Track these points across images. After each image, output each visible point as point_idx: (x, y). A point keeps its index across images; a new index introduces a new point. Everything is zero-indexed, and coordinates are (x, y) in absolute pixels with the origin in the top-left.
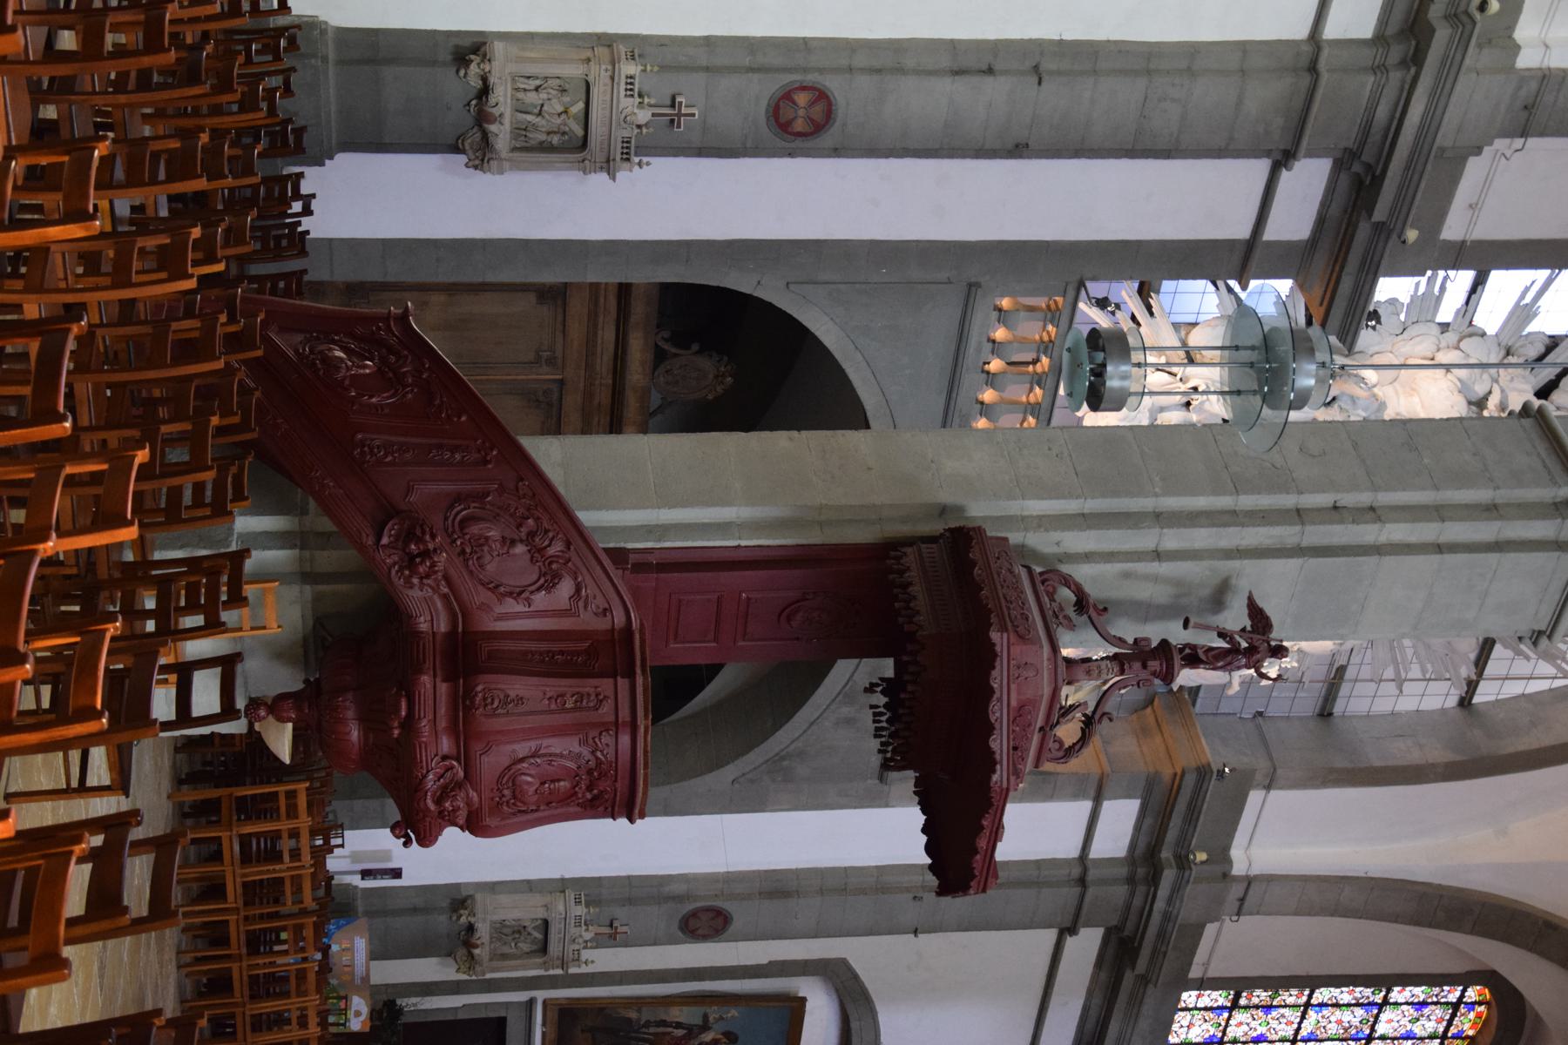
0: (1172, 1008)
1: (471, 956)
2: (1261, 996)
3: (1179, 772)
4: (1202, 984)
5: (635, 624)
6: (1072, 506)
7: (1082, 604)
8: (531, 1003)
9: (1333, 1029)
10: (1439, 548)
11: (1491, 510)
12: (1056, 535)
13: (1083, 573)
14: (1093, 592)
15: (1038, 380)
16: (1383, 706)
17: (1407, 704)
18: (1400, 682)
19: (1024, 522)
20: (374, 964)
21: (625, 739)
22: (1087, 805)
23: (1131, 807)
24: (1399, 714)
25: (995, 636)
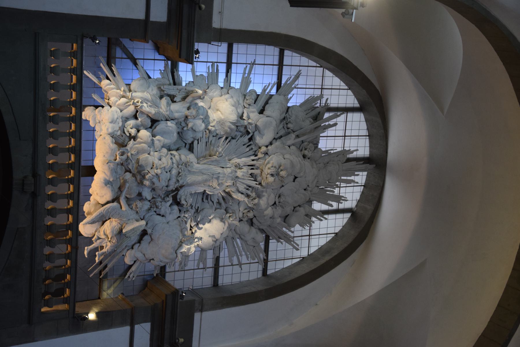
3: (164, 298)
16: (236, 279)
17: (245, 278)
22: (128, 328)
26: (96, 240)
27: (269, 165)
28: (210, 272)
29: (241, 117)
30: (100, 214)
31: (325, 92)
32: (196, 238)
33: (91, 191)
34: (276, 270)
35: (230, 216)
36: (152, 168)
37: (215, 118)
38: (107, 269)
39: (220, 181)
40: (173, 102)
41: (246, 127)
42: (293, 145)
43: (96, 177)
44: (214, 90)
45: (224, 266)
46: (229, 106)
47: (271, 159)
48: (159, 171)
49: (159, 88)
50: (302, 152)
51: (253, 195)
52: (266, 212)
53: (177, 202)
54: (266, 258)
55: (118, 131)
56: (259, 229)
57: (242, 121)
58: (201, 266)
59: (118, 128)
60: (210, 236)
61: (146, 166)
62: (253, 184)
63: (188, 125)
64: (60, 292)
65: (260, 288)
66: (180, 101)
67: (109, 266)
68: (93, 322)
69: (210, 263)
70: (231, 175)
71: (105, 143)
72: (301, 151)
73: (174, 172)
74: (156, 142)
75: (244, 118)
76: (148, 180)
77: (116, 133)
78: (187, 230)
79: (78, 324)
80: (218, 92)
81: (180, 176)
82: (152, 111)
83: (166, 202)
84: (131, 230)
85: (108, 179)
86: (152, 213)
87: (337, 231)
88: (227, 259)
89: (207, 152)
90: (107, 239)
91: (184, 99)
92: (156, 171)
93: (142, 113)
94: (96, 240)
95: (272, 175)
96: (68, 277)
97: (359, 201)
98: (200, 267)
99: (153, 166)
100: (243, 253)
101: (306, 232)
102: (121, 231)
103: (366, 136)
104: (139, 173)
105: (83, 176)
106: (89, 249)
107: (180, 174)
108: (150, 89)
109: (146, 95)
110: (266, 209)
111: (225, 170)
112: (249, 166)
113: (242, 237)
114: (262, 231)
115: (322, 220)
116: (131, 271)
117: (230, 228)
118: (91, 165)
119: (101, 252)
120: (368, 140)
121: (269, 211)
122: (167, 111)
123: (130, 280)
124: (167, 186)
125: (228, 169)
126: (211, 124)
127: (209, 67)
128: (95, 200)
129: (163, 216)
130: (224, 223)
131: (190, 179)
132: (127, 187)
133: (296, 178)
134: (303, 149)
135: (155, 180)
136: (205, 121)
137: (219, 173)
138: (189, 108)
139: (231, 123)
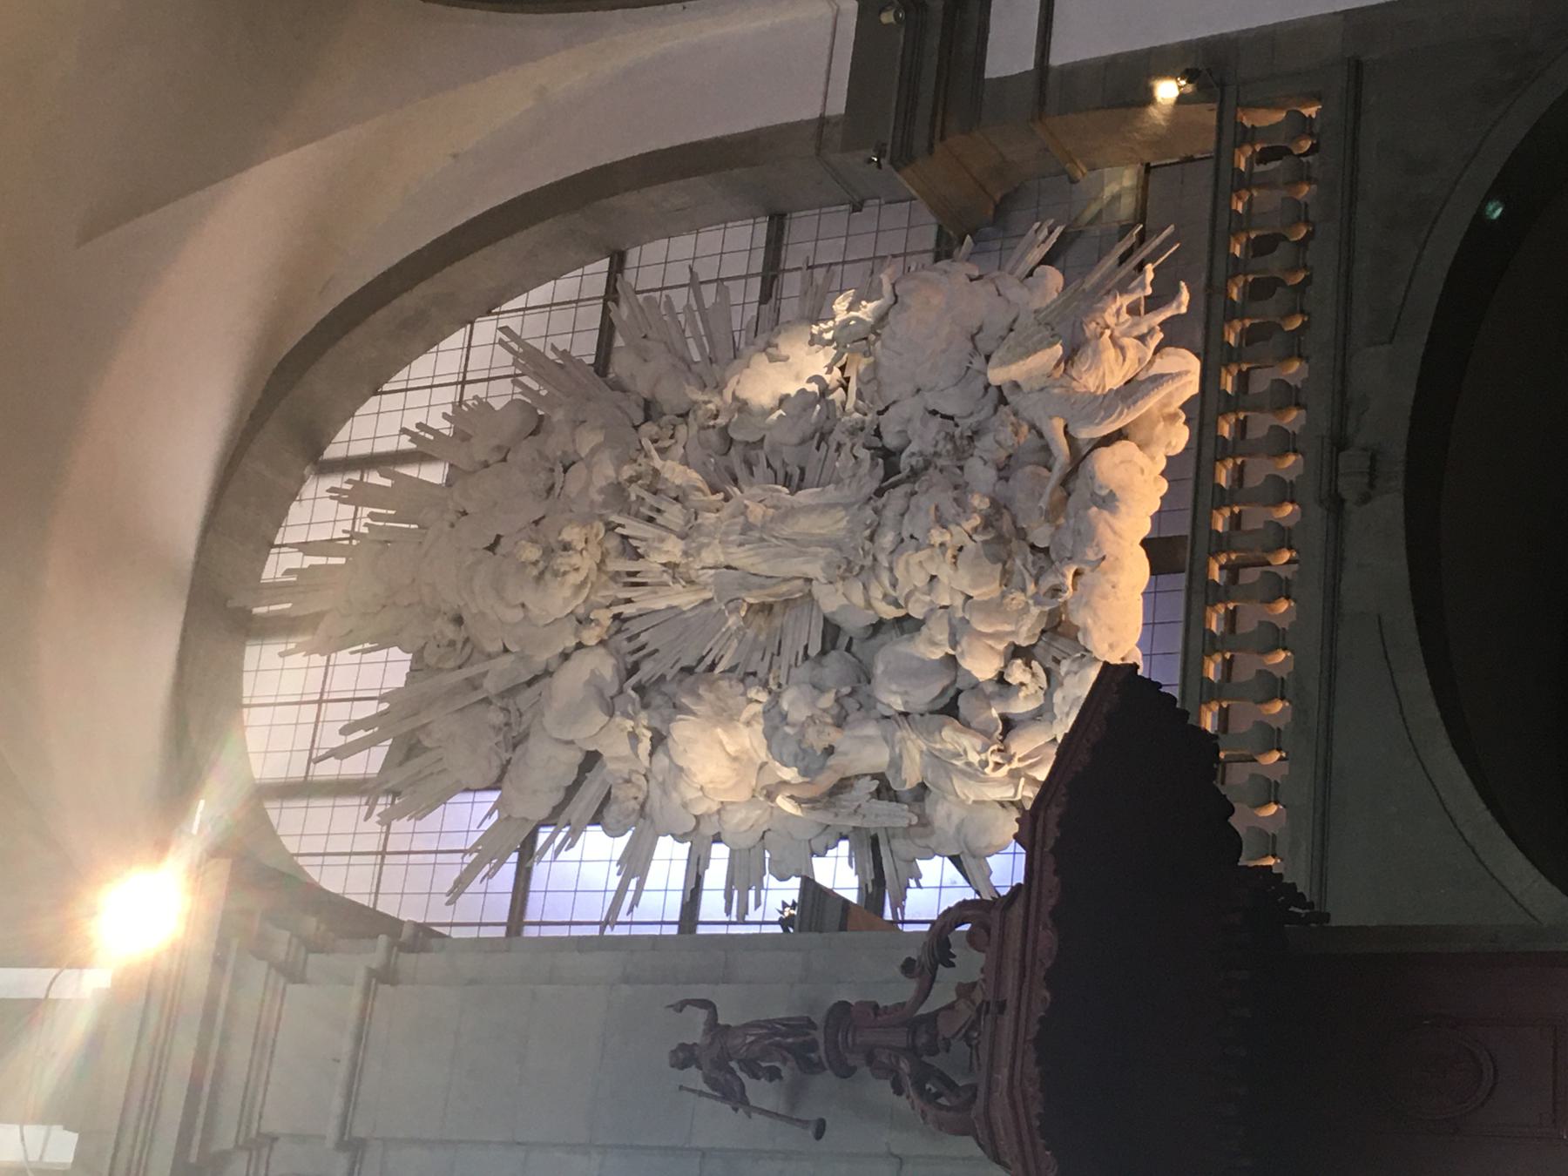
3: (938, 147)
10: (570, 923)
15: (1239, 224)
16: (710, 239)
17: (683, 245)
18: (695, 284)
22: (1056, 60)
24: (689, 232)
26: (1151, 331)
27: (575, 578)
28: (792, 257)
29: (659, 740)
30: (1135, 403)
31: (373, 844)
32: (829, 343)
33: (1164, 486)
34: (579, 272)
35: (716, 417)
36: (961, 549)
37: (745, 731)
38: (1122, 251)
39: (741, 519)
40: (879, 776)
41: (645, 706)
42: (490, 656)
43: (1145, 528)
44: (744, 828)
45: (746, 277)
46: (694, 768)
47: (566, 601)
48: (937, 536)
49: (925, 823)
50: (463, 634)
51: (634, 491)
52: (596, 438)
53: (888, 457)
54: (611, 304)
55: (1067, 673)
56: (624, 391)
57: (657, 724)
58: (819, 274)
59: (1067, 682)
60: (787, 358)
61: (977, 556)
62: (633, 528)
63: (837, 700)
64: (1261, 247)
65: (630, 200)
66: (857, 777)
67: (1111, 261)
68: (1165, 74)
69: (791, 284)
70: (706, 540)
71: (1111, 629)
72: (467, 640)
73: (887, 539)
74: (943, 637)
75: (649, 734)
76: (975, 510)
77: (1075, 667)
78: (859, 379)
79: (1210, 66)
80: (737, 819)
81: (868, 527)
82: (952, 738)
83: (921, 454)
84: (1035, 351)
85: (1106, 514)
86: (966, 425)
87: (374, 400)
88: (736, 296)
89: (777, 622)
90: (1117, 333)
91: (843, 785)
92: (947, 538)
93: (986, 734)
94: (1151, 331)
95: (566, 547)
96: (1235, 294)
97: (293, 496)
98: (824, 270)
99: (955, 557)
100: (681, 318)
101: (470, 391)
102: (1069, 358)
103: (249, 706)
104: (1004, 540)
105: (1182, 538)
106: (1174, 305)
107: (867, 532)
108: (955, 820)
109: (968, 791)
110: (593, 451)
111: (722, 559)
112: (644, 584)
113: (682, 366)
114: (617, 386)
115: (419, 425)
116: (1046, 248)
117: (719, 387)
118: (1161, 577)
119: (1138, 295)
120: (247, 692)
121: (588, 440)
122: (903, 740)
123: (1051, 221)
124: (913, 493)
125: (710, 561)
126: (758, 708)
127: (757, 905)
128: (1152, 458)
129: (934, 413)
130: (735, 398)
131: (834, 524)
132: (1046, 498)
133: (492, 548)
134: (459, 646)
135: (950, 509)
136: (777, 720)
137: (741, 545)
138: (830, 751)
139: (693, 713)
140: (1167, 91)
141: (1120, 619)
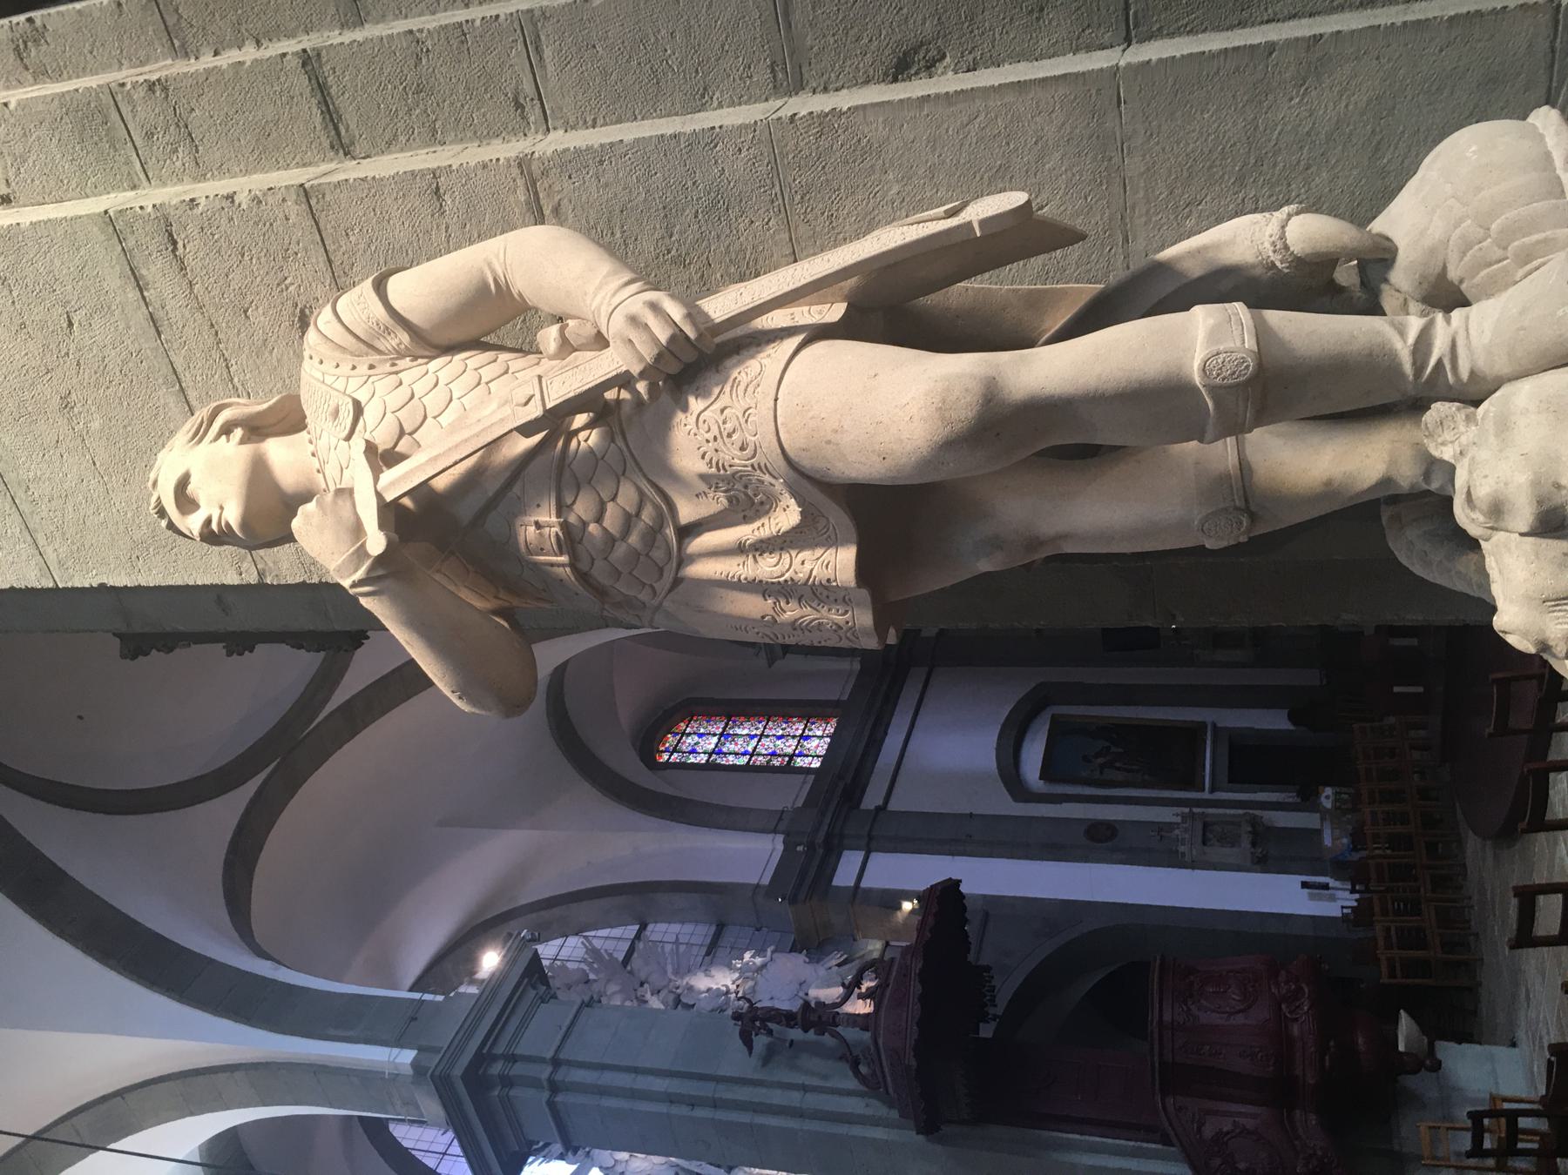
0: (826, 759)
1: (1253, 826)
2: (776, 762)
4: (807, 771)
5: (1158, 1098)
6: (857, 1131)
7: (855, 1065)
8: (1212, 790)
9: (740, 741)
10: (636, 1070)
11: (603, 1091)
12: (869, 1112)
13: (852, 1083)
14: (845, 1067)
16: (688, 928)
18: (677, 942)
19: (888, 1124)
20: (1318, 826)
21: (1167, 1017)
22: (864, 884)
23: (838, 881)
25: (914, 1063)
140: (907, 906)
141: (1122, 63)
